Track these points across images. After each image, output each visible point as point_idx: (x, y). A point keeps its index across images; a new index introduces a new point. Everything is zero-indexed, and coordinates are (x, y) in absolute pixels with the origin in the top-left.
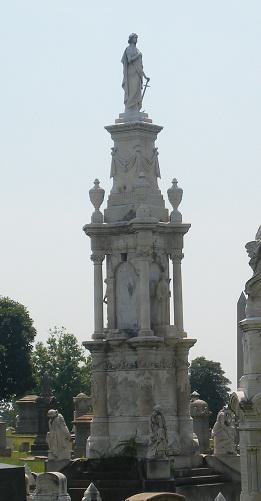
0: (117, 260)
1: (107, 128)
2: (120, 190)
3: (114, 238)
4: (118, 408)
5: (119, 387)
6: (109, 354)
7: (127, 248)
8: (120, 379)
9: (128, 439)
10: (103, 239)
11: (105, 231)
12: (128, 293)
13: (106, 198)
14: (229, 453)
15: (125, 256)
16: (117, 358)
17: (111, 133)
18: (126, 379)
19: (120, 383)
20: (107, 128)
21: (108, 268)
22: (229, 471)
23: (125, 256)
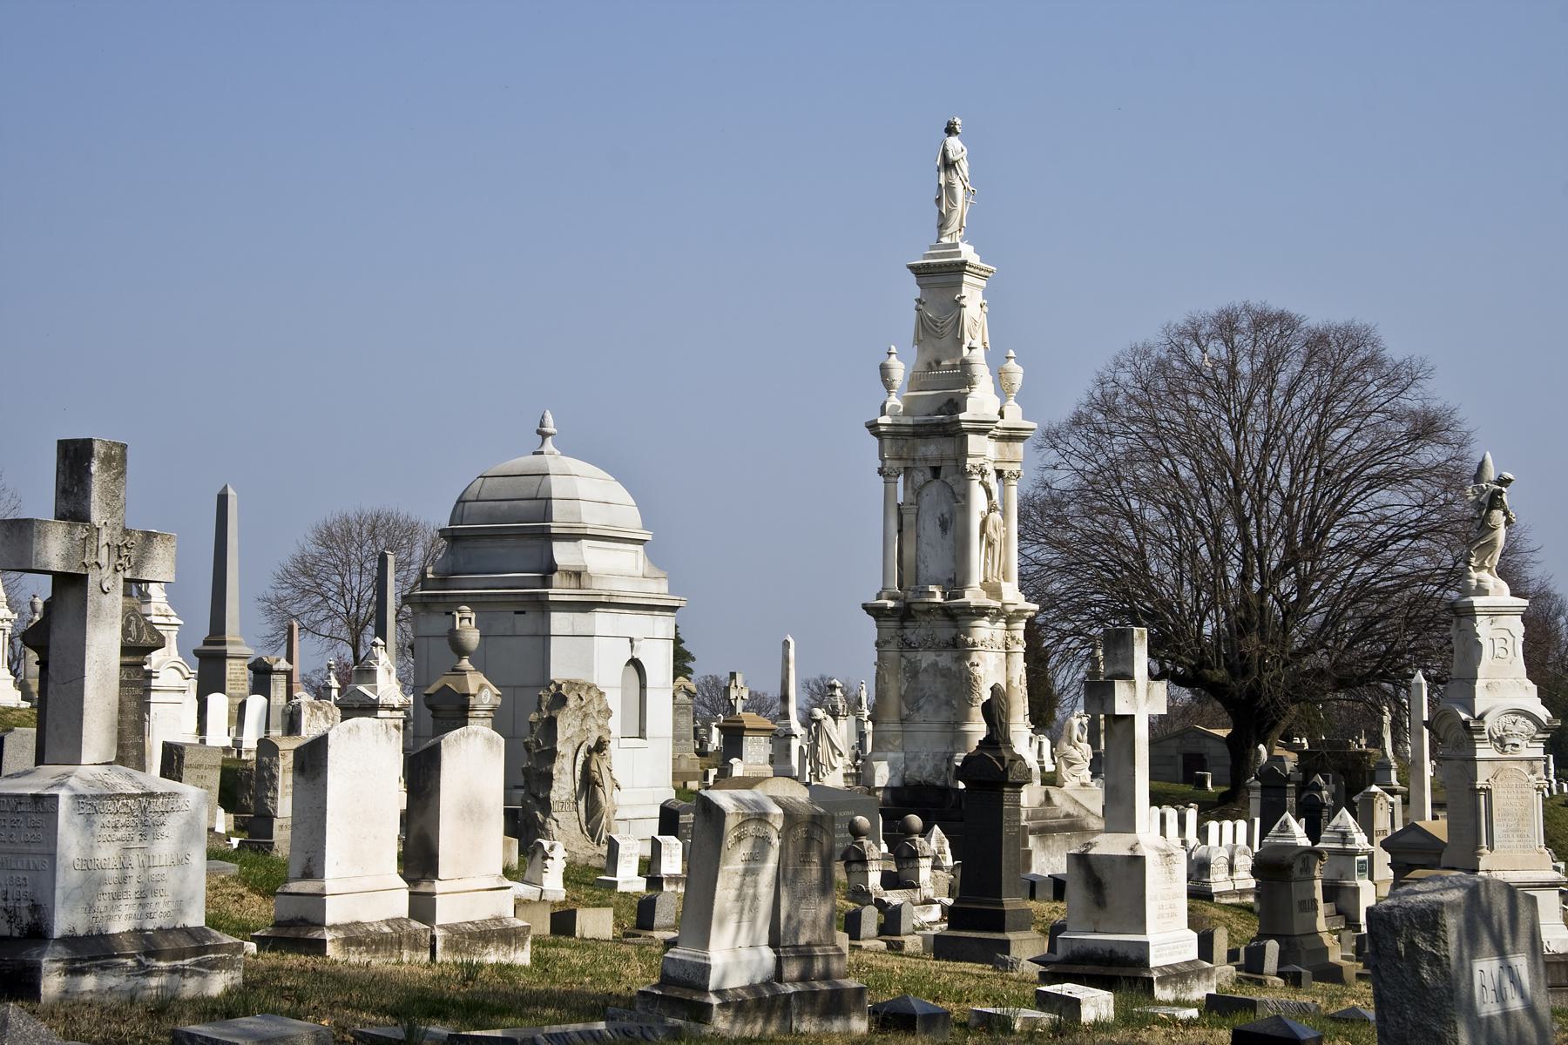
0: (919, 478)
1: (911, 267)
2: (929, 364)
3: (918, 441)
4: (918, 709)
5: (922, 677)
6: (906, 624)
7: (942, 460)
8: (924, 665)
9: (761, 874)
10: (901, 443)
11: (906, 430)
12: (939, 528)
13: (865, 705)
14: (1083, 785)
15: (936, 471)
16: (922, 632)
17: (877, 618)
18: (935, 664)
19: (925, 670)
20: (911, 267)
21: (905, 489)
22: (1083, 813)
23: (936, 471)
